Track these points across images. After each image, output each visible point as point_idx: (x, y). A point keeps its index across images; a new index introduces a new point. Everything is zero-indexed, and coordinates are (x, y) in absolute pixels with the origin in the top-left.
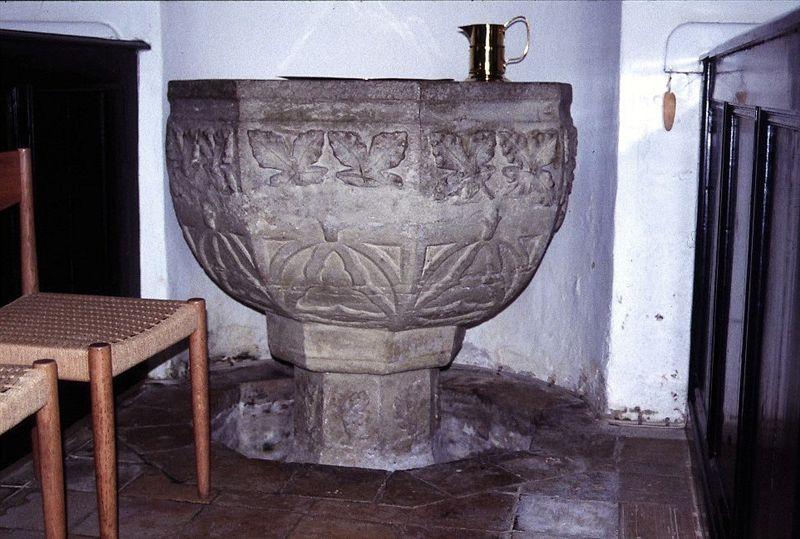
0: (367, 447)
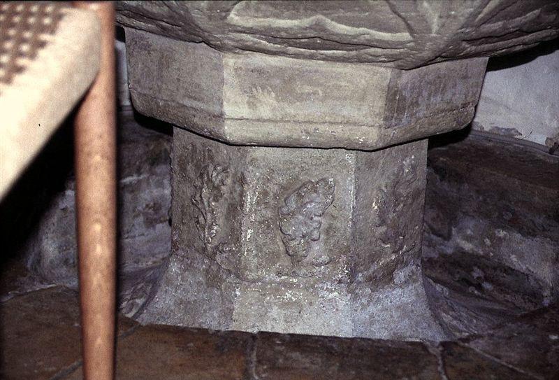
0: (325, 278)
